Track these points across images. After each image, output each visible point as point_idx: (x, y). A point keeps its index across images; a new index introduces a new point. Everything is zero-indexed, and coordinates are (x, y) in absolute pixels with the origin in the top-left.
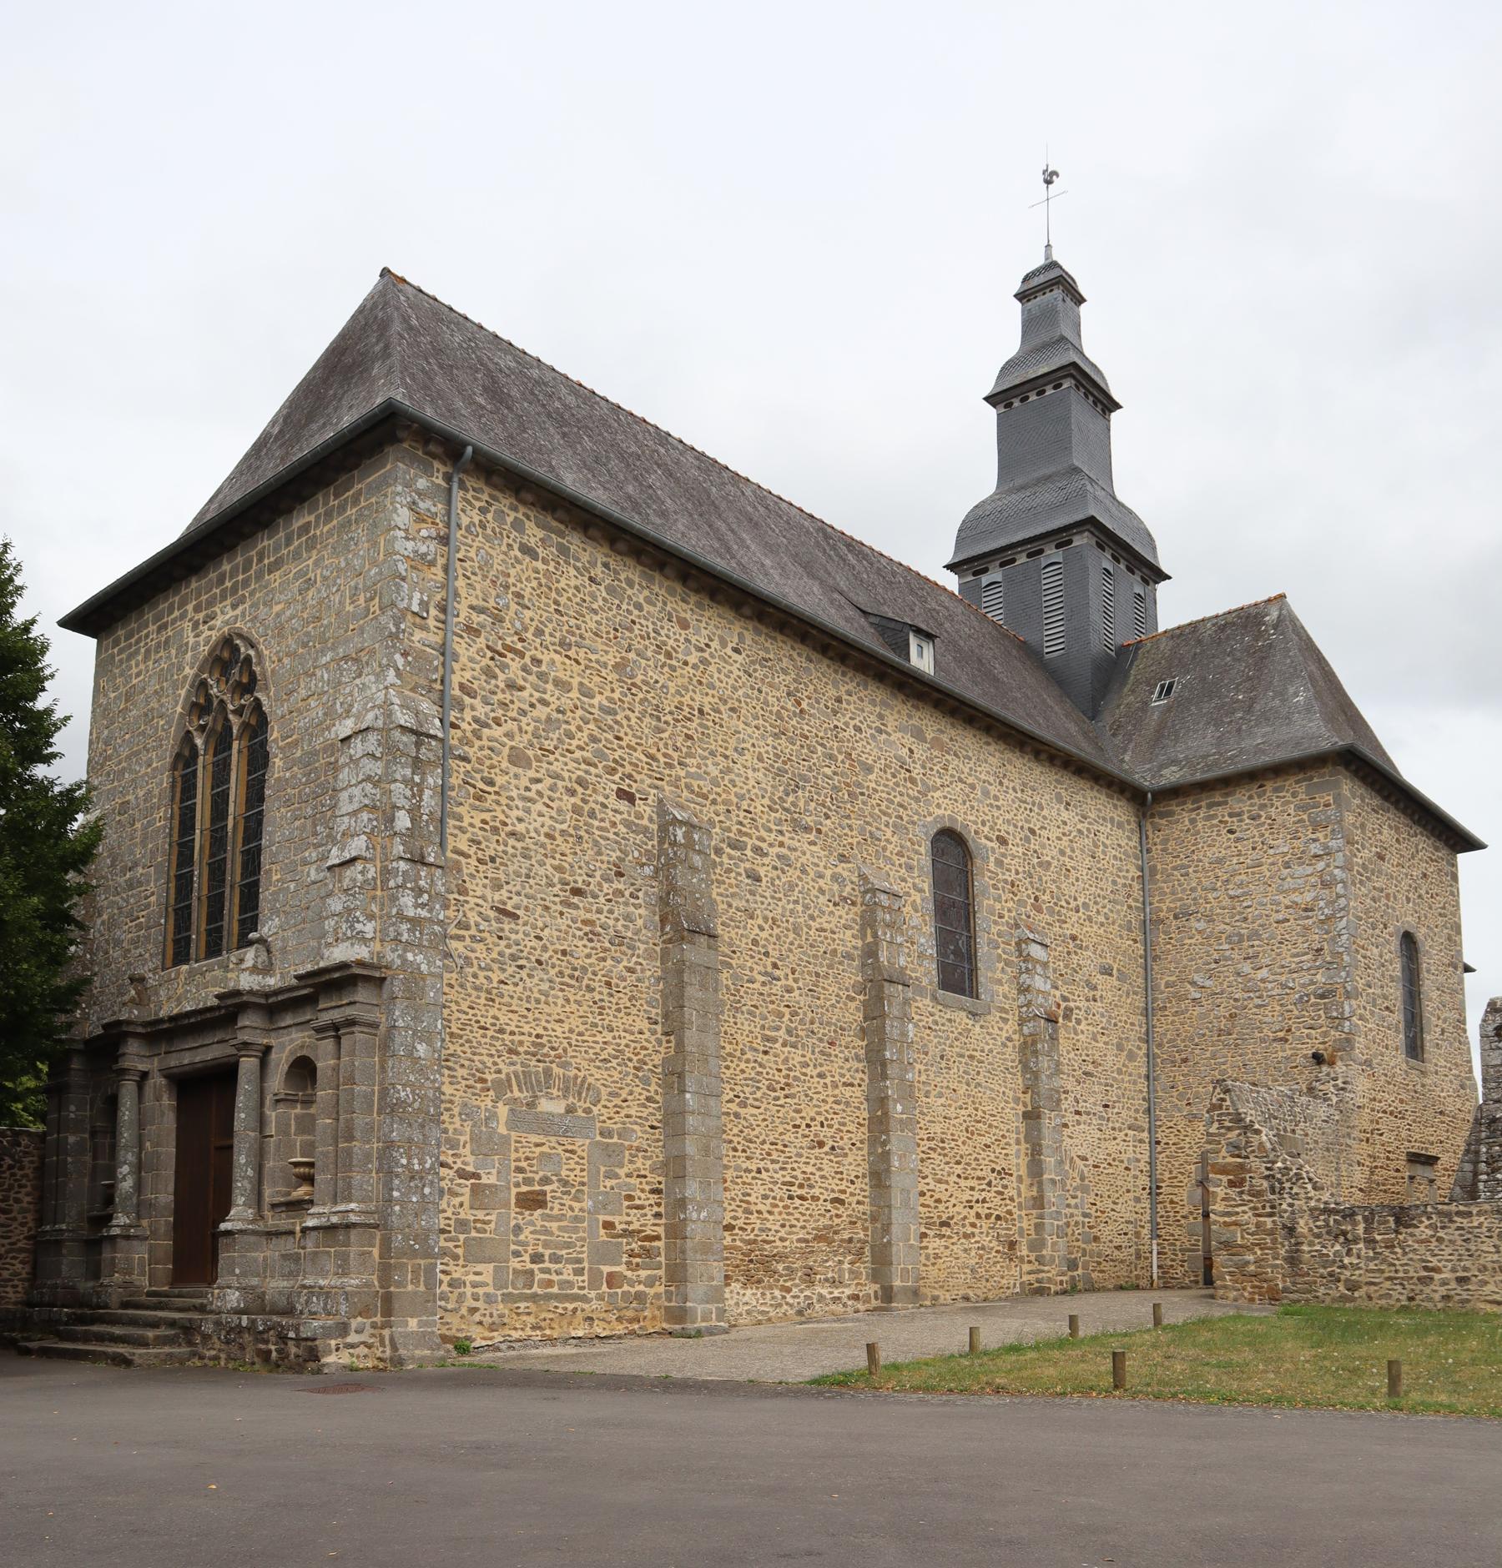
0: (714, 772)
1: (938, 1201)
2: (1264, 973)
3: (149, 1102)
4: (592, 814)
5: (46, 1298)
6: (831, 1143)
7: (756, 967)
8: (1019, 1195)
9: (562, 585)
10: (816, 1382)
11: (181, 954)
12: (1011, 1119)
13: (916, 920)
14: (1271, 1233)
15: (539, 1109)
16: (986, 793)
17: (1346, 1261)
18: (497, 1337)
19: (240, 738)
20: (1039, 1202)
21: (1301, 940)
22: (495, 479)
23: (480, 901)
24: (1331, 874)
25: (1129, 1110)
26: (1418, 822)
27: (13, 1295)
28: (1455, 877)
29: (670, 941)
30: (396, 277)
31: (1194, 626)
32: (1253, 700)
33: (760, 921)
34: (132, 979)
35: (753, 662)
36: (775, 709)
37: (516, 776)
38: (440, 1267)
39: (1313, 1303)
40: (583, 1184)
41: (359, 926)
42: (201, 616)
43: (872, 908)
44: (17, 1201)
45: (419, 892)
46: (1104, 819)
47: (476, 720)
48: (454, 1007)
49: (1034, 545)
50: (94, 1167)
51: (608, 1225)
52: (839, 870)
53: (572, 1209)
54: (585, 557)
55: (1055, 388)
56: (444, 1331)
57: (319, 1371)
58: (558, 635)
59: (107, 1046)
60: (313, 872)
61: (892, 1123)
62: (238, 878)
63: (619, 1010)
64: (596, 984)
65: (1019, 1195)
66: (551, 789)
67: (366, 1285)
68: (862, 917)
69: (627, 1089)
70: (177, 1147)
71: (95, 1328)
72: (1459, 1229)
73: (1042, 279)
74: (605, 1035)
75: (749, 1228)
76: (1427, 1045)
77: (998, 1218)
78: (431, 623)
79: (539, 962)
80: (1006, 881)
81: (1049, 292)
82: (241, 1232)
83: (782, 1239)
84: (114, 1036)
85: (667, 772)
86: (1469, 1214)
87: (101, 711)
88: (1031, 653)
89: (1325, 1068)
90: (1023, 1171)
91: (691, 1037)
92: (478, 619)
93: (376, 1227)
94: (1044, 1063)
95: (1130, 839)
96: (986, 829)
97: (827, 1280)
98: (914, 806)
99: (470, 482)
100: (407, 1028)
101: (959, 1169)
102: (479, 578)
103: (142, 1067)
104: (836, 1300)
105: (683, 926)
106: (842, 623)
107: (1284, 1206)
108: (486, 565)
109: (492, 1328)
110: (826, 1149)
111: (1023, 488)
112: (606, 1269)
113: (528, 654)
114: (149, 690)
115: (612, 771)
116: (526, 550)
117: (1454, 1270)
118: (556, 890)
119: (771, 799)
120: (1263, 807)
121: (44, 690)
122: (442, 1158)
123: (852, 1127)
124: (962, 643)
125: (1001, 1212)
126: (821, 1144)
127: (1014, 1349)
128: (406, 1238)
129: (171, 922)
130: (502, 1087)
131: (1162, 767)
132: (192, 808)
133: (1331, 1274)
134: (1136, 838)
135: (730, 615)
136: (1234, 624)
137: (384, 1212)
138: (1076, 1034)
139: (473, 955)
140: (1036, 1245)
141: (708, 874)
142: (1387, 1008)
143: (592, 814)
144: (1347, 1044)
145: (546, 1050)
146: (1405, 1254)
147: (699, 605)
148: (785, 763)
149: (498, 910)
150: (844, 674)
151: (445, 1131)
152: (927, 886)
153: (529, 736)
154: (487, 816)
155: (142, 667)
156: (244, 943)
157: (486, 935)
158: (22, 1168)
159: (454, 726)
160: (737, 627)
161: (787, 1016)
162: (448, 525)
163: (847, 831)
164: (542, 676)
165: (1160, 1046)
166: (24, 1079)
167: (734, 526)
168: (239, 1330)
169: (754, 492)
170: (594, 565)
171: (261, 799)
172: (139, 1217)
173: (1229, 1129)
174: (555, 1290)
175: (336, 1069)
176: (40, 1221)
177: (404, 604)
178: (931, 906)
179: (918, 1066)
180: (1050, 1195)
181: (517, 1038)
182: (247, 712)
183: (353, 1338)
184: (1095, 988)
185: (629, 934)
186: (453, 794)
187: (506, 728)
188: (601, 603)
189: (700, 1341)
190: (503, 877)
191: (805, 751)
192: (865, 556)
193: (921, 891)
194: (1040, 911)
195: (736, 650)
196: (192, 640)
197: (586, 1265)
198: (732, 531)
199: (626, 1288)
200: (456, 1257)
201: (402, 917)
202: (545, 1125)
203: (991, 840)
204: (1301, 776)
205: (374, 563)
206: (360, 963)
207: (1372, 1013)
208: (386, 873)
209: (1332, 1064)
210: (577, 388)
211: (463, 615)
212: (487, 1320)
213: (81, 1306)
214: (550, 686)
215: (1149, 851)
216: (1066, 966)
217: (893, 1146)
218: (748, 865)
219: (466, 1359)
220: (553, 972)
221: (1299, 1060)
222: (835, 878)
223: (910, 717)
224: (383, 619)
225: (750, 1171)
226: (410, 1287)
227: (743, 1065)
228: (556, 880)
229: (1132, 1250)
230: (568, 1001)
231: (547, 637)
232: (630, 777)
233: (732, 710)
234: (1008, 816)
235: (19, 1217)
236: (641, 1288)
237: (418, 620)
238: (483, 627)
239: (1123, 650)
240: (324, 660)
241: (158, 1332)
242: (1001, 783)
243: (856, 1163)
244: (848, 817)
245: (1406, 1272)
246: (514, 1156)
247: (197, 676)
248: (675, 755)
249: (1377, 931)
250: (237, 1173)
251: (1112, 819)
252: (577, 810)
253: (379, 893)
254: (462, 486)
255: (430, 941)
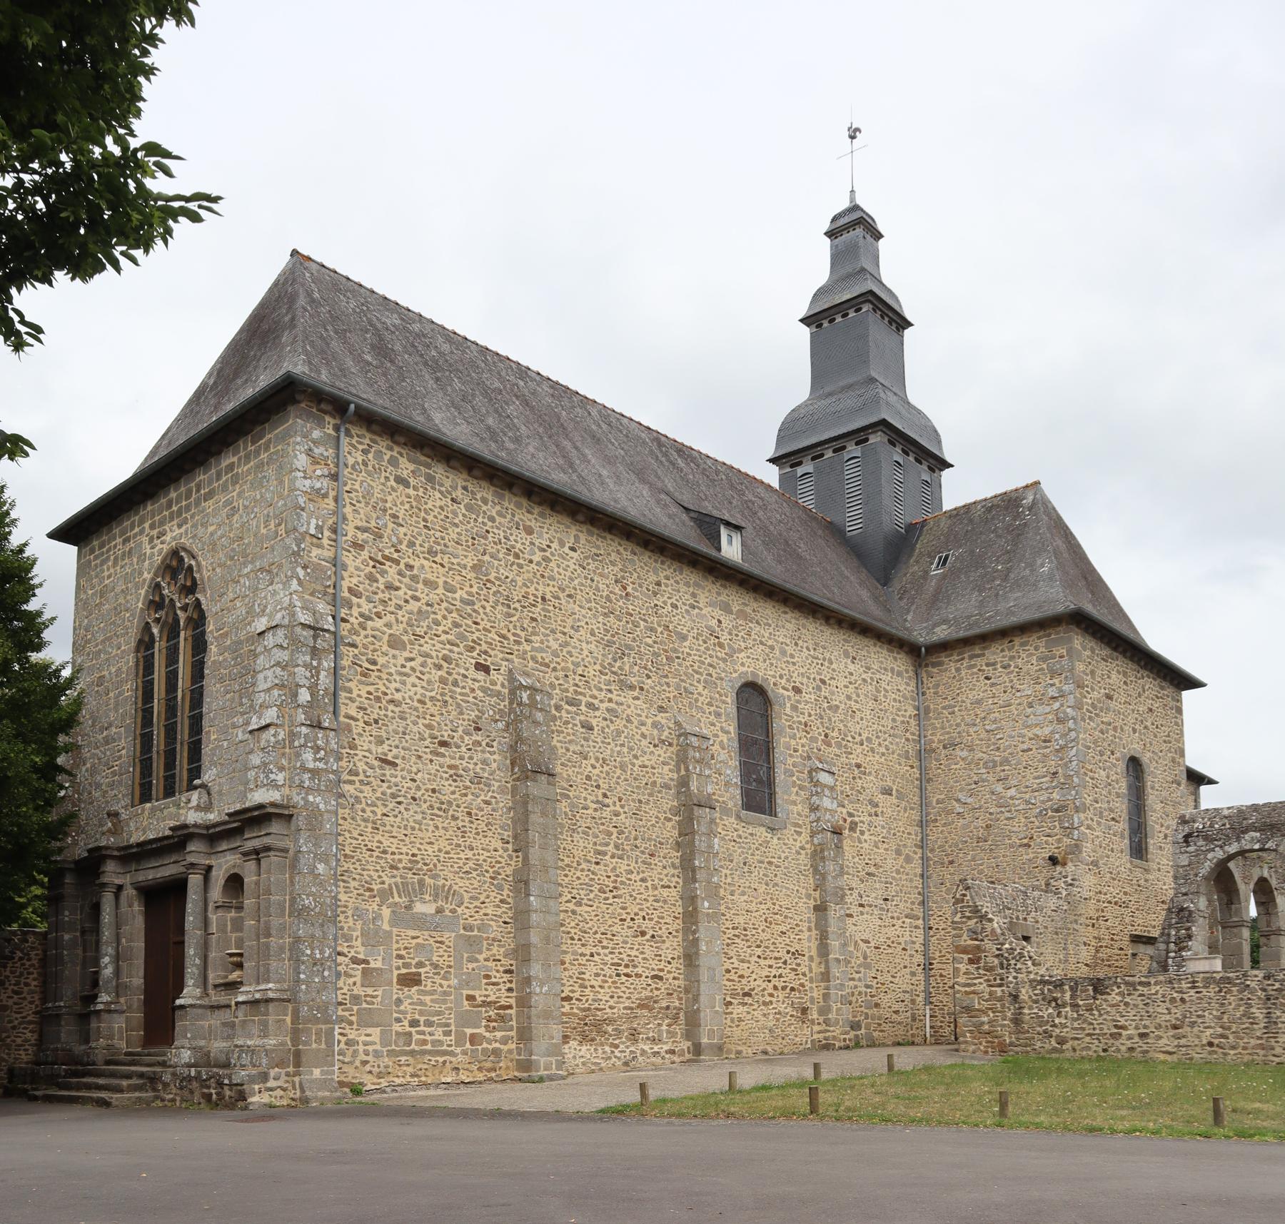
0: (555, 645)
1: (742, 976)
2: (1012, 792)
3: (124, 908)
4: (455, 683)
5: (50, 1059)
6: (651, 932)
7: (589, 797)
8: (811, 971)
9: (430, 506)
10: (602, 1111)
11: (145, 796)
12: (804, 911)
13: (723, 756)
14: (1000, 999)
15: (415, 910)
16: (783, 653)
17: (1057, 1021)
18: (384, 1083)
19: (185, 629)
20: (826, 976)
21: (1041, 765)
22: (374, 427)
23: (367, 754)
24: (1065, 712)
25: (906, 902)
26: (1145, 667)
27: (25, 1057)
28: (1179, 711)
29: (518, 779)
30: (303, 256)
31: (967, 508)
32: (1009, 570)
33: (593, 761)
34: (109, 815)
35: (586, 558)
36: (605, 594)
37: (394, 657)
38: (337, 1031)
39: (1032, 1054)
40: (450, 967)
41: (272, 776)
42: (155, 532)
43: (686, 748)
44: (27, 984)
45: (317, 749)
46: (885, 669)
47: (362, 615)
48: (347, 835)
49: (838, 443)
50: (84, 957)
51: (471, 998)
52: (658, 718)
53: (441, 985)
54: (448, 483)
55: (857, 311)
56: (342, 1078)
57: (246, 1108)
58: (426, 545)
59: (92, 864)
60: (240, 734)
61: (700, 916)
62: (186, 737)
63: (478, 834)
64: (459, 814)
65: (811, 971)
66: (422, 666)
67: (281, 1044)
68: (677, 755)
69: (485, 894)
70: (146, 942)
71: (84, 1080)
72: (1141, 995)
73: (846, 220)
74: (469, 855)
75: (584, 999)
76: (1151, 848)
77: (792, 989)
78: (325, 542)
79: (414, 799)
80: (800, 723)
81: (853, 230)
82: (192, 1006)
83: (611, 1007)
84: (96, 858)
85: (516, 647)
86: (1149, 984)
87: (82, 605)
88: (836, 531)
89: (1059, 868)
90: (814, 953)
91: (534, 853)
92: (362, 536)
93: (289, 1001)
94: (831, 867)
95: (908, 684)
96: (783, 681)
97: (648, 1038)
98: (722, 665)
99: (355, 430)
100: (309, 852)
101: (759, 951)
102: (362, 505)
103: (117, 881)
104: (656, 1054)
105: (529, 767)
106: (665, 519)
107: (1010, 979)
108: (368, 494)
109: (380, 1075)
110: (648, 937)
111: (830, 394)
112: (469, 1031)
113: (403, 562)
114: (118, 589)
115: (472, 649)
116: (399, 480)
117: (1137, 1028)
118: (427, 743)
119: (602, 665)
120: (1012, 658)
121: (34, 595)
122: (339, 949)
123: (669, 920)
124: (772, 528)
125: (795, 984)
126: (643, 934)
127: (764, 1088)
128: (311, 1009)
129: (138, 770)
130: (385, 895)
131: (935, 626)
132: (151, 682)
133: (1045, 1032)
134: (913, 683)
135: (567, 521)
136: (998, 506)
137: (294, 990)
138: (860, 842)
139: (361, 795)
140: (824, 1011)
141: (548, 726)
142: (1113, 819)
143: (455, 683)
144: (1077, 848)
145: (419, 866)
146: (1101, 1015)
147: (542, 515)
148: (613, 636)
149: (382, 760)
150: (663, 563)
151: (342, 928)
152: (732, 728)
153: (404, 625)
154: (371, 689)
155: (112, 570)
156: (191, 788)
157: (372, 779)
158: (29, 960)
159: (344, 620)
160: (573, 531)
161: (615, 835)
162: (337, 465)
163: (665, 687)
164: (414, 578)
165: (932, 851)
166: (33, 888)
167: (579, 444)
168: (189, 1079)
169: (600, 412)
170: (455, 488)
171: (202, 677)
172: (118, 995)
173: (969, 918)
174: (429, 1047)
175: (257, 883)
176: (44, 1000)
177: (303, 529)
178: (736, 744)
179: (724, 871)
180: (835, 971)
181: (397, 857)
182: (190, 609)
183: (271, 1084)
184: (877, 806)
185: (486, 775)
186: (344, 672)
187: (385, 620)
188: (461, 518)
189: (540, 1085)
190: (384, 735)
191: (630, 625)
192: (693, 460)
193: (728, 732)
194: (829, 745)
195: (572, 549)
196: (148, 551)
197: (453, 1028)
198: (576, 448)
199: (485, 1045)
200: (351, 1023)
201: (304, 769)
202: (420, 922)
203: (787, 690)
204: (1042, 633)
205: (281, 497)
206: (273, 805)
207: (1099, 823)
208: (292, 735)
209: (1064, 864)
210: (452, 338)
211: (350, 534)
212: (376, 1070)
213: (77, 1064)
214: (420, 586)
215: (924, 694)
216: (852, 789)
217: (702, 934)
218: (582, 718)
219: (359, 1099)
220: (425, 806)
221: (1040, 862)
222: (655, 725)
223: (719, 594)
224: (288, 541)
225: (585, 955)
226: (314, 1046)
227: (579, 874)
228: (426, 736)
229: (909, 1014)
230: (437, 827)
231: (418, 548)
232: (486, 653)
233: (570, 596)
234: (802, 670)
235: (29, 997)
236: (497, 1045)
237: (315, 540)
238: (367, 542)
239: (911, 528)
240: (246, 571)
241: (130, 1082)
242: (796, 644)
243: (672, 947)
244: (666, 676)
245: (1101, 1029)
246: (395, 946)
247: (153, 579)
248: (523, 634)
249: (1105, 757)
250: (188, 962)
251: (892, 670)
252: (443, 681)
253: (287, 750)
254: (348, 434)
255: (326, 786)
